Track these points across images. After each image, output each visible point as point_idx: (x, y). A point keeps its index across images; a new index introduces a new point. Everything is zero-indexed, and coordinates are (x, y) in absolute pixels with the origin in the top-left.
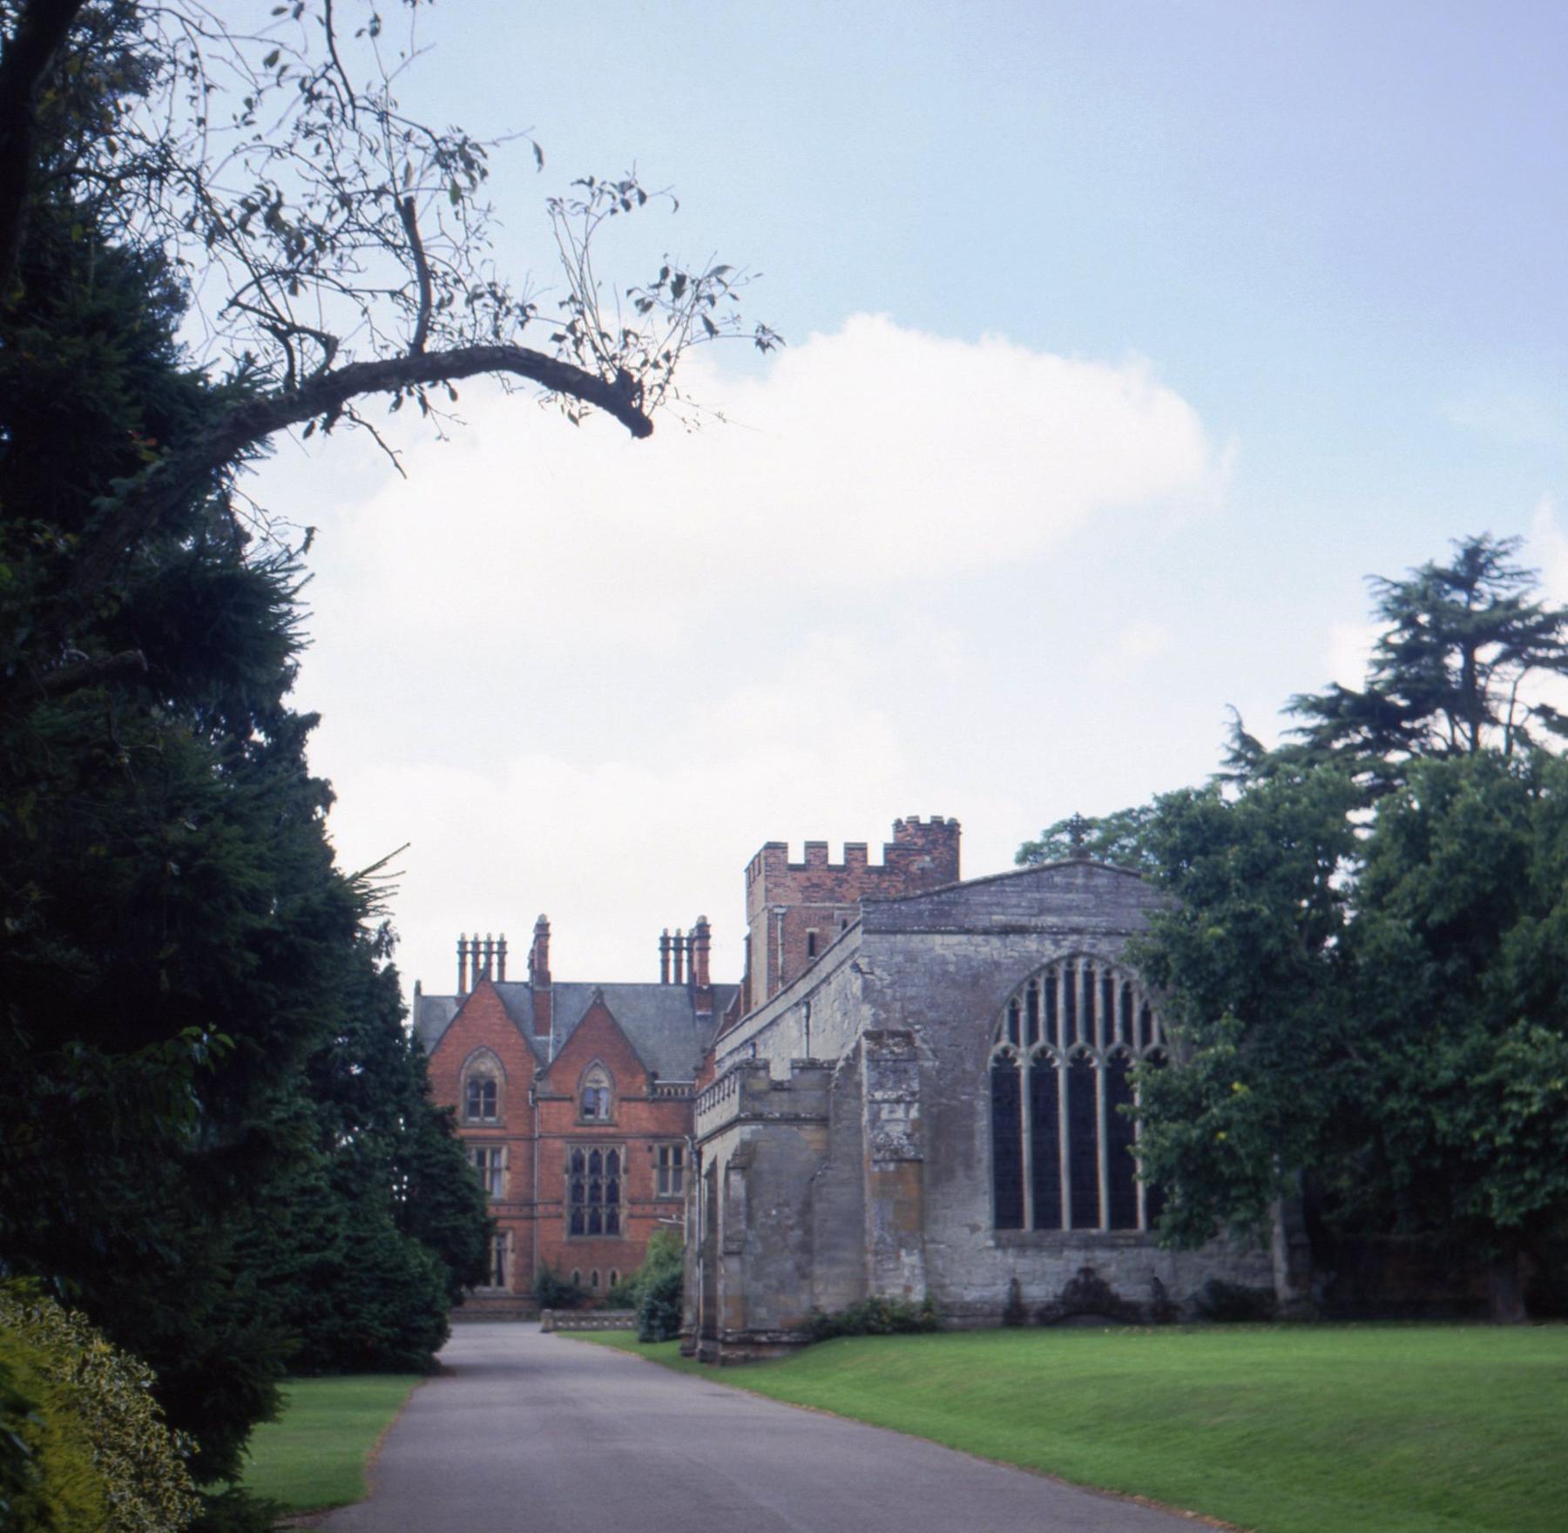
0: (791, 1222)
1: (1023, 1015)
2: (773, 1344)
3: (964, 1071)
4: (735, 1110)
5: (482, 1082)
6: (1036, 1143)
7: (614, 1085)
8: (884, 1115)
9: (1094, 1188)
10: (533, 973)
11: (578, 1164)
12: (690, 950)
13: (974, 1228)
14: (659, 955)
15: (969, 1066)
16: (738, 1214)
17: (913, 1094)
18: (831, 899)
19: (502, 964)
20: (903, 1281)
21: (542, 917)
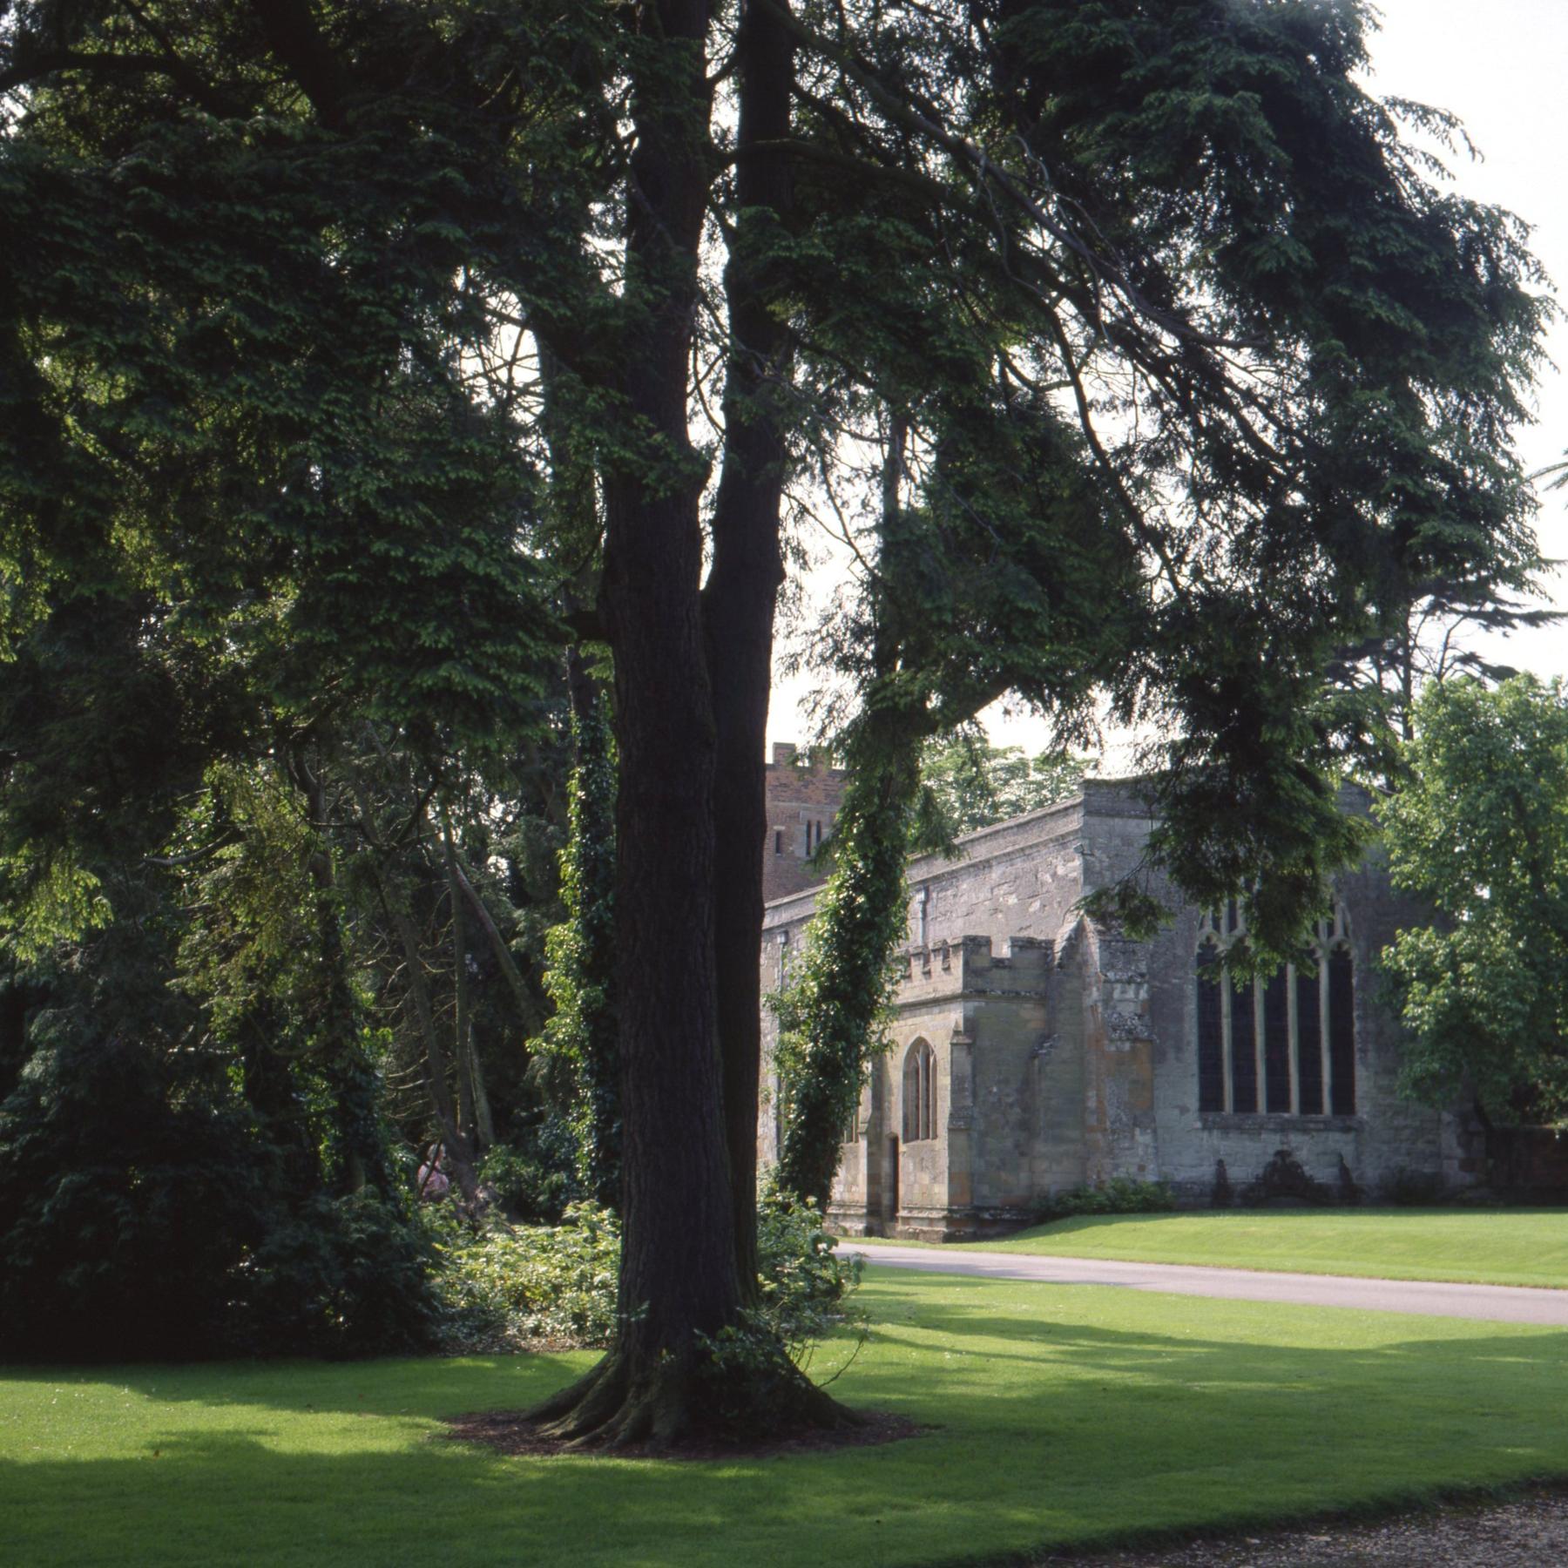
0: (1010, 1100)
2: (994, 1222)
3: (1175, 956)
6: (1235, 1028)
8: (1116, 995)
9: (1286, 1073)
13: (1184, 1110)
15: (1180, 951)
16: (964, 1090)
17: (1142, 975)
18: (798, 799)
20: (1137, 1160)
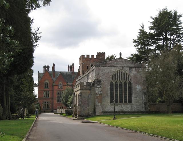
1: (114, 77)
4: (79, 88)
5: (47, 83)
7: (63, 84)
10: (52, 70)
11: (58, 93)
12: (72, 67)
14: (68, 68)
19: (49, 69)
21: (54, 63)
